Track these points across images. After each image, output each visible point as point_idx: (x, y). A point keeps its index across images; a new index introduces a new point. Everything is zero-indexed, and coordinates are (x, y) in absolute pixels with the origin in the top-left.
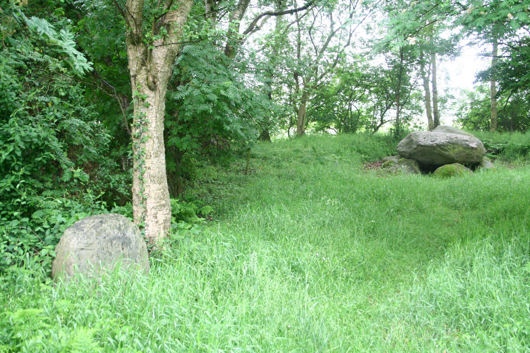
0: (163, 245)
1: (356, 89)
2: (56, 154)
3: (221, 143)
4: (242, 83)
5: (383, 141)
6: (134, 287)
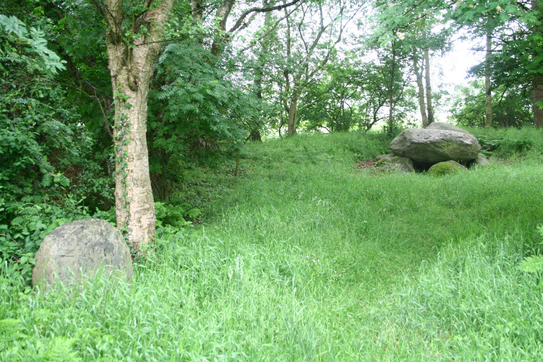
0: (147, 251)
1: (348, 86)
2: (35, 158)
3: (209, 144)
4: (228, 82)
5: (376, 138)
6: (116, 295)
